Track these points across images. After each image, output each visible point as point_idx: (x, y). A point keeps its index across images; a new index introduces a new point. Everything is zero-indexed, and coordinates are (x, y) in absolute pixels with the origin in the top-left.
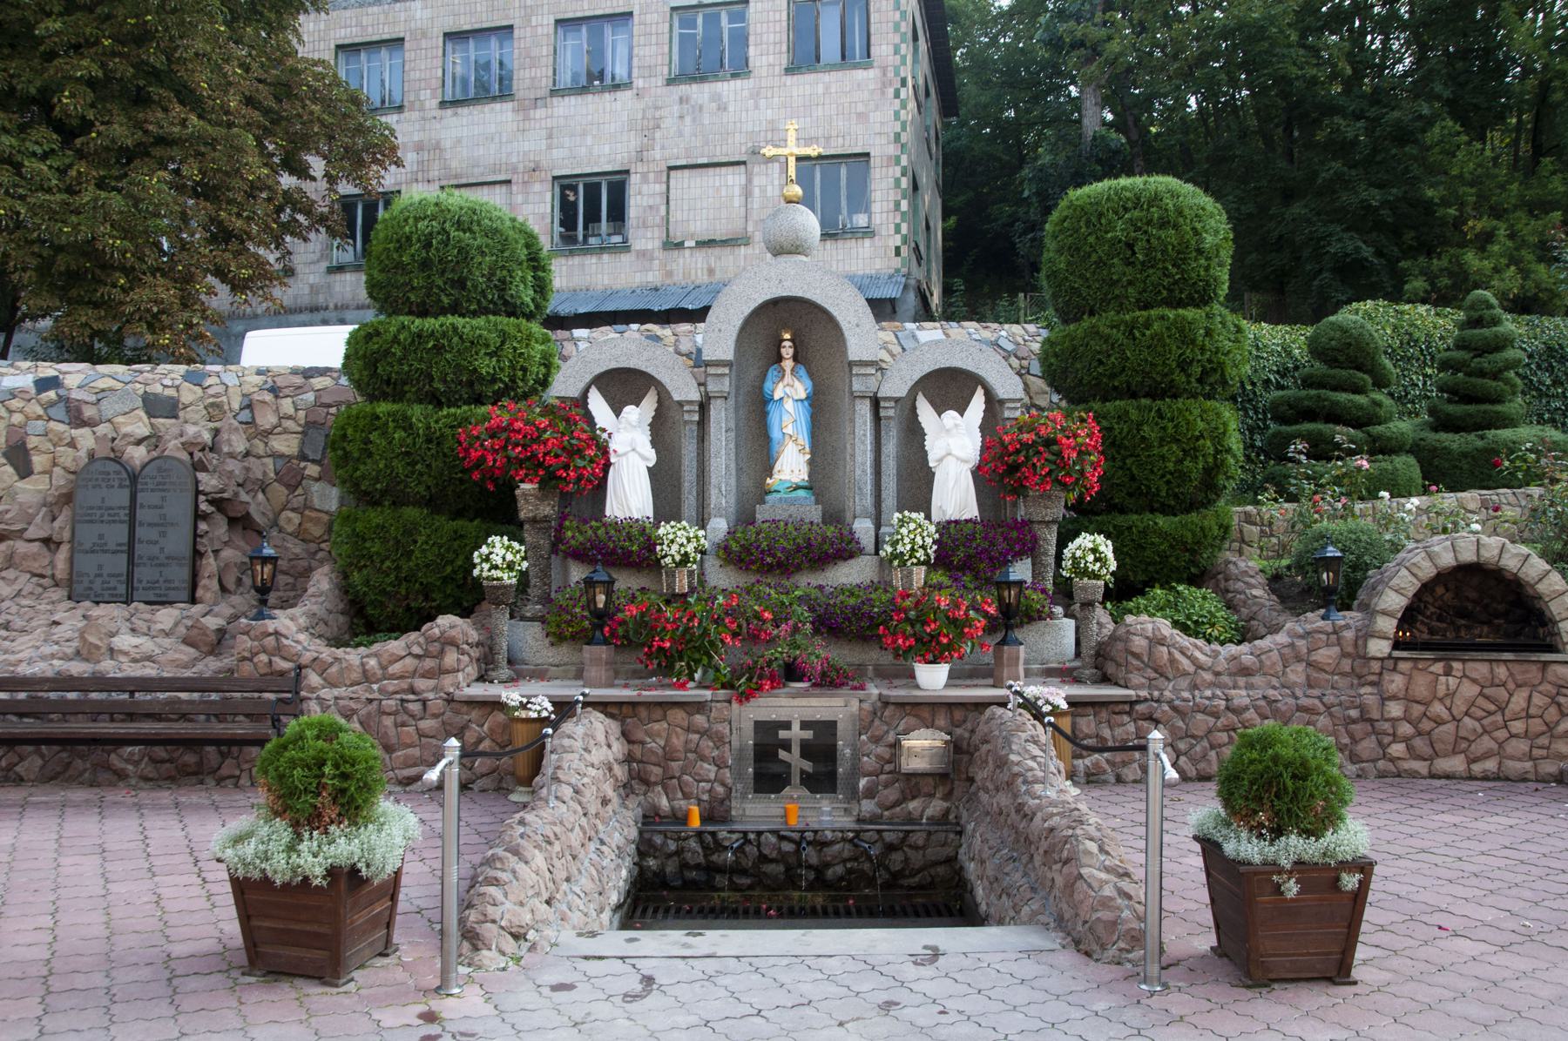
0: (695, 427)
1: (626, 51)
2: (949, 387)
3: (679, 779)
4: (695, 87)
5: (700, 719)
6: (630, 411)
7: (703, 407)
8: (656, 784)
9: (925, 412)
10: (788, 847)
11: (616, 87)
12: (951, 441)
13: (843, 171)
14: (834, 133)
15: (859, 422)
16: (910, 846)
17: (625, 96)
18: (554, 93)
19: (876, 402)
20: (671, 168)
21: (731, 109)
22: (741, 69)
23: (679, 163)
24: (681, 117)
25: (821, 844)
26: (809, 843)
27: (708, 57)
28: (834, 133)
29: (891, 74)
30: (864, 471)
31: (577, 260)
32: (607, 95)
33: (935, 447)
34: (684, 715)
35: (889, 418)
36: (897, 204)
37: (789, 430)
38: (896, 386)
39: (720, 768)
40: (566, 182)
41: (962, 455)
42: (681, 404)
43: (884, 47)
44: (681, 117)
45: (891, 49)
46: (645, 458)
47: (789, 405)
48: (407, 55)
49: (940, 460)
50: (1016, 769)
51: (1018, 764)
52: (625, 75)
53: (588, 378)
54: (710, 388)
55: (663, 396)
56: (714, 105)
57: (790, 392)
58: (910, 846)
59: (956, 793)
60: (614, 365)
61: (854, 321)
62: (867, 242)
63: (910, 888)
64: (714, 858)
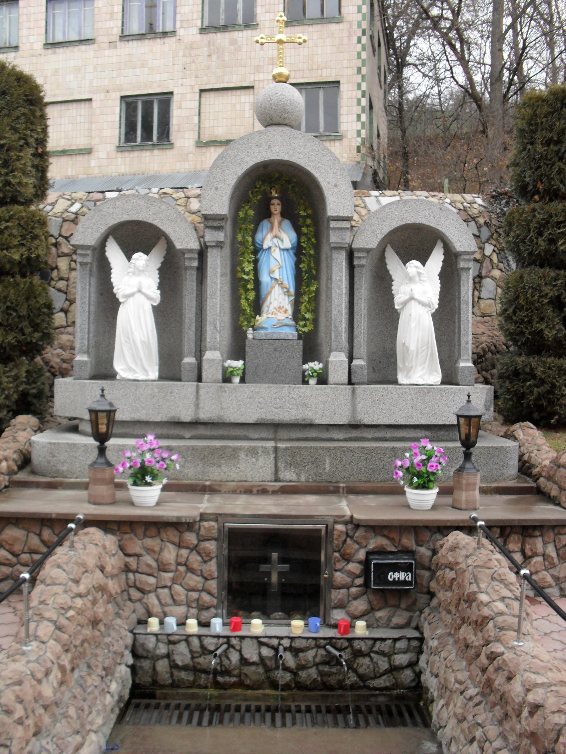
0: (195, 272)
1: (172, 9)
2: (414, 242)
3: (170, 588)
4: (219, 35)
5: (191, 538)
6: (139, 258)
7: (202, 254)
8: (150, 592)
9: (393, 263)
10: (266, 652)
11: (165, 34)
12: (413, 286)
13: (321, 94)
14: (315, 67)
15: (335, 269)
16: (376, 652)
17: (170, 41)
18: (124, 37)
19: (351, 254)
20: (202, 91)
21: (244, 50)
22: (250, 23)
23: (207, 87)
24: (210, 56)
25: (295, 651)
26: (285, 649)
27: (228, 17)
28: (315, 67)
29: (355, 26)
30: (340, 312)
31: (136, 154)
32: (158, 40)
33: (401, 292)
34: (176, 533)
35: (362, 266)
36: (359, 117)
37: (276, 275)
38: (369, 239)
39: (206, 579)
40: (130, 100)
41: (424, 299)
42: (183, 252)
43: (351, 8)
44: (210, 56)
45: (356, 9)
46: (149, 298)
47: (276, 253)
48: (21, 10)
49: (405, 303)
50: (486, 612)
51: (487, 604)
52: (172, 26)
53: (103, 229)
54: (207, 238)
55: (170, 245)
56: (232, 47)
57: (278, 242)
58: (376, 652)
59: (419, 604)
60: (125, 218)
61: (333, 182)
62: (337, 143)
63: (375, 689)
64: (201, 660)
